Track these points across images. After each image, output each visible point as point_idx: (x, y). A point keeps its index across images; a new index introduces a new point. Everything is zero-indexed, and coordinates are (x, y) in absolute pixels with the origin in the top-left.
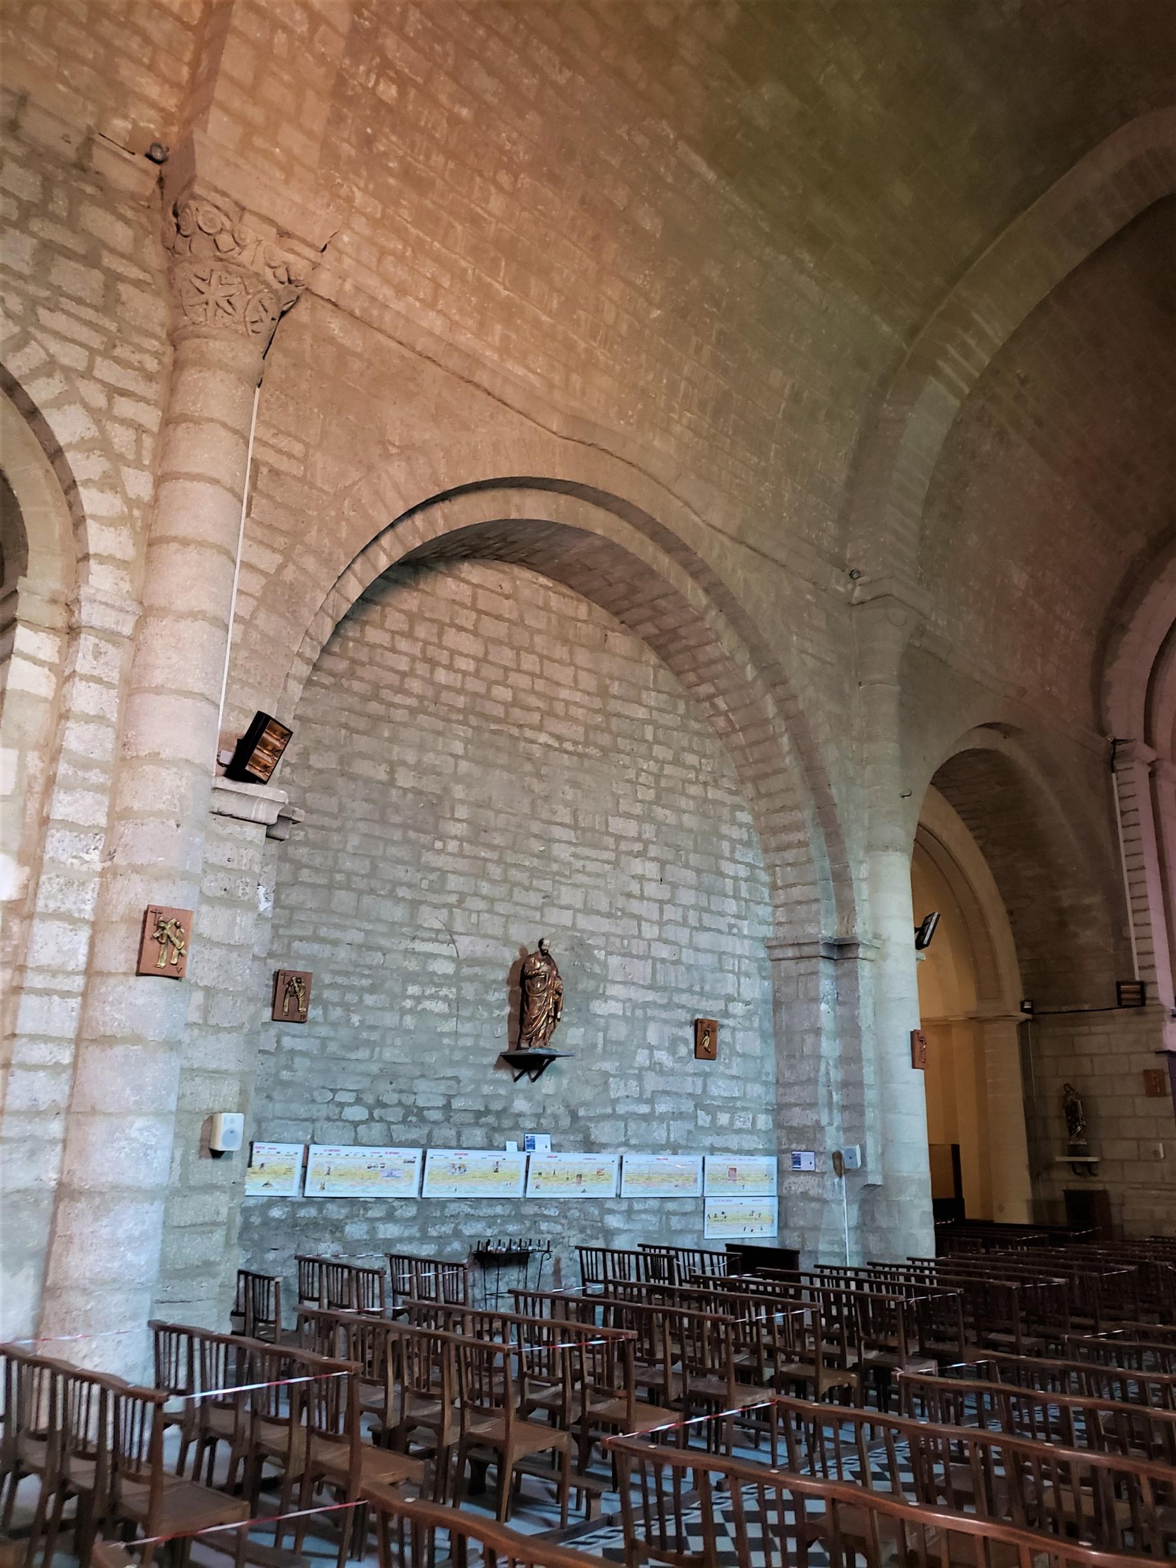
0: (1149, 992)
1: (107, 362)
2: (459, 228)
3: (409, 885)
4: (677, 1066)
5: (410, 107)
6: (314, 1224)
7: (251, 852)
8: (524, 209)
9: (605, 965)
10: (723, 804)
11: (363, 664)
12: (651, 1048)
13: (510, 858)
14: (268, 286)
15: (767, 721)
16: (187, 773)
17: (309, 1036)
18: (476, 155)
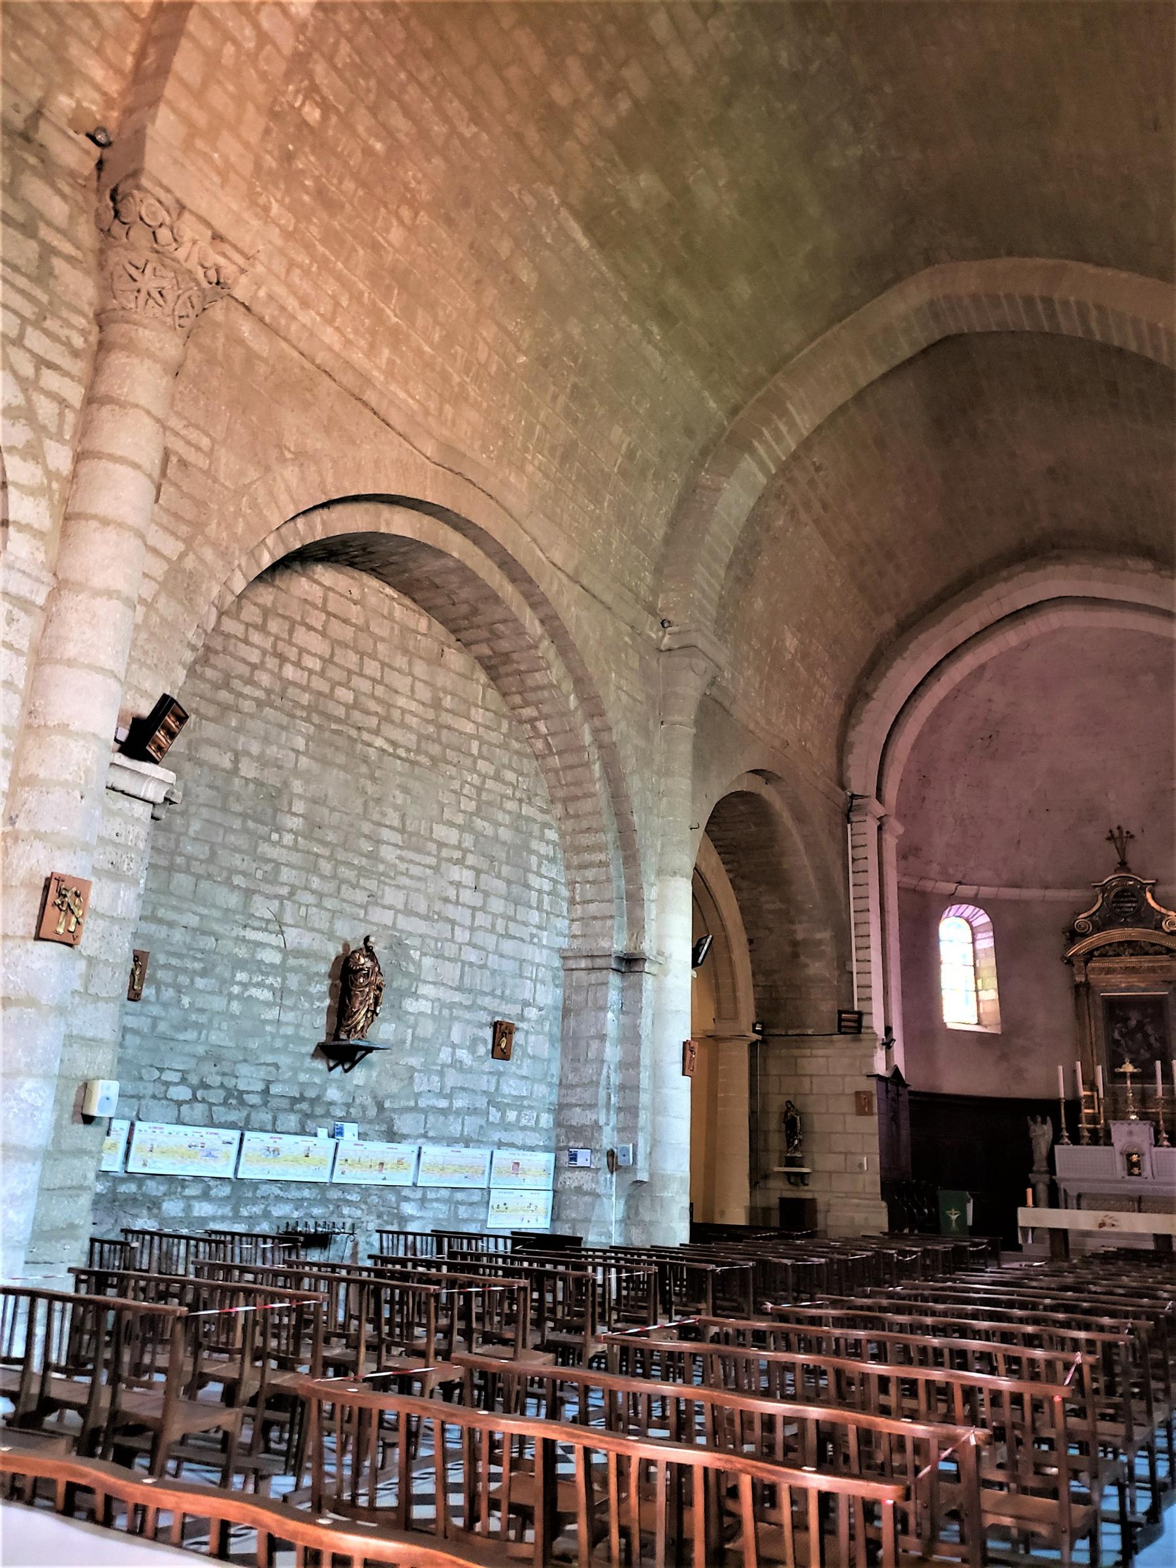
0: (865, 1021)
1: (38, 333)
2: (361, 252)
3: (244, 874)
4: (475, 1064)
5: (330, 132)
6: (133, 1200)
7: (138, 829)
8: (419, 244)
9: (418, 965)
10: (534, 820)
11: (216, 652)
12: (454, 1046)
13: (341, 855)
14: (198, 284)
15: (581, 749)
16: (94, 747)
17: (141, 1014)
18: (384, 187)
